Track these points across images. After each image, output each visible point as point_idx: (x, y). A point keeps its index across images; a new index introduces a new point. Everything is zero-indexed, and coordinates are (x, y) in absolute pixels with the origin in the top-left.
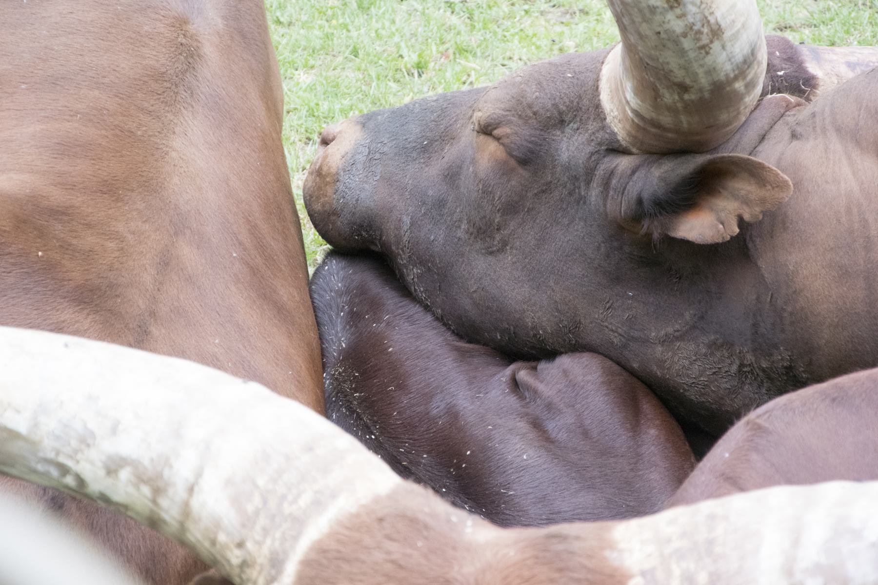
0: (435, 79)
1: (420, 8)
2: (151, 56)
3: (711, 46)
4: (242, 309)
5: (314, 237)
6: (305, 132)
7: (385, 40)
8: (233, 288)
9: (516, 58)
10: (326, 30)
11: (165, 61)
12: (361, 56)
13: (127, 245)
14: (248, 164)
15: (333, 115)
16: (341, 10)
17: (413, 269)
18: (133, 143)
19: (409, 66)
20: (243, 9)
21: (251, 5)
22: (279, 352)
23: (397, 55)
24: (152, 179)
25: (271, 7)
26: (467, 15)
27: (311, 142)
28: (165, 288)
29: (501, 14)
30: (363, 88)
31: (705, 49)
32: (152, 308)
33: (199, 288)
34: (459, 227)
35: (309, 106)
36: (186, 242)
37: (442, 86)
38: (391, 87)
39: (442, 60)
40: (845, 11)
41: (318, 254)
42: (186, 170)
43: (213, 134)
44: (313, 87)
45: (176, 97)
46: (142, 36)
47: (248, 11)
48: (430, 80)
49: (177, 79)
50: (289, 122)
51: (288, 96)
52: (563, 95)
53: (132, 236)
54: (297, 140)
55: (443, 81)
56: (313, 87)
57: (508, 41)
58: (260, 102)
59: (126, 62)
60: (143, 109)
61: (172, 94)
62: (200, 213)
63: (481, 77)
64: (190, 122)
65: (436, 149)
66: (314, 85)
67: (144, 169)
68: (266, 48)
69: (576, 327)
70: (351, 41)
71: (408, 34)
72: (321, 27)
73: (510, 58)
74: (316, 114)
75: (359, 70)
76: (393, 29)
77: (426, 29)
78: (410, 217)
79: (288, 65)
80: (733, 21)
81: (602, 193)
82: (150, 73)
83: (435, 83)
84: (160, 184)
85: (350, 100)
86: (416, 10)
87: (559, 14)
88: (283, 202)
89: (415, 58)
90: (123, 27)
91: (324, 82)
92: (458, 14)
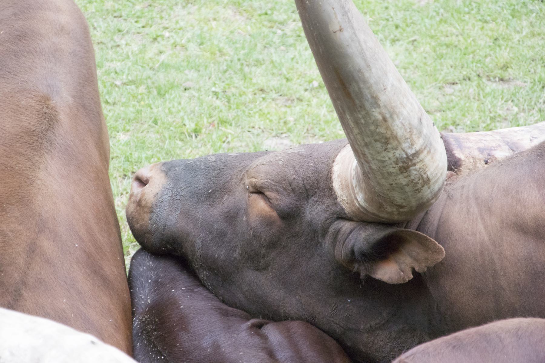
0: (205, 140)
1: (196, 95)
2: (26, 120)
3: (423, 189)
4: (81, 280)
5: (128, 237)
6: (123, 172)
7: (175, 114)
8: (75, 266)
9: (257, 127)
10: (137, 108)
11: (35, 124)
12: (159, 124)
13: (8, 239)
14: (86, 188)
15: (141, 161)
16: (147, 95)
17: (203, 272)
18: (13, 175)
19: (189, 131)
20: (86, 92)
21: (90, 89)
22: (104, 307)
23: (182, 124)
24: (25, 197)
25: (103, 93)
26: (226, 100)
27: (127, 177)
28: (32, 267)
29: (248, 100)
30: (160, 144)
31: (419, 190)
32: (23, 279)
33: (54, 266)
34: (235, 251)
35: (126, 155)
36: (46, 237)
37: (210, 144)
38: (178, 144)
39: (211, 127)
40: (462, 102)
41: (130, 247)
42: (46, 191)
43: (65, 169)
44: (129, 143)
45: (41, 146)
46: (20, 108)
47: (88, 93)
48: (203, 139)
49: (42, 134)
50: (113, 165)
51: (112, 148)
52: (308, 179)
53: (12, 233)
54: (117, 176)
55: (211, 141)
56: (129, 143)
57: (252, 116)
58: (95, 150)
59: (10, 124)
60: (19, 153)
61: (38, 144)
62: (55, 219)
63: (235, 138)
64: (50, 162)
65: (217, 196)
66: (129, 142)
67: (20, 191)
68: (100, 116)
69: (313, 320)
70: (153, 115)
71: (189, 111)
72: (134, 106)
73: (253, 127)
74: (130, 160)
75: (158, 133)
76: (180, 108)
77: (200, 108)
78: (201, 240)
79: (113, 130)
80: (437, 174)
81: (332, 243)
82: (24, 131)
83: (205, 142)
84: (30, 201)
85: (152, 151)
86: (194, 96)
87: (284, 100)
88: (109, 213)
89: (193, 126)
90: (9, 102)
91: (136, 140)
92: (221, 99)
